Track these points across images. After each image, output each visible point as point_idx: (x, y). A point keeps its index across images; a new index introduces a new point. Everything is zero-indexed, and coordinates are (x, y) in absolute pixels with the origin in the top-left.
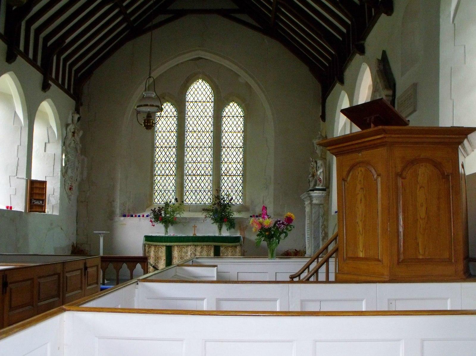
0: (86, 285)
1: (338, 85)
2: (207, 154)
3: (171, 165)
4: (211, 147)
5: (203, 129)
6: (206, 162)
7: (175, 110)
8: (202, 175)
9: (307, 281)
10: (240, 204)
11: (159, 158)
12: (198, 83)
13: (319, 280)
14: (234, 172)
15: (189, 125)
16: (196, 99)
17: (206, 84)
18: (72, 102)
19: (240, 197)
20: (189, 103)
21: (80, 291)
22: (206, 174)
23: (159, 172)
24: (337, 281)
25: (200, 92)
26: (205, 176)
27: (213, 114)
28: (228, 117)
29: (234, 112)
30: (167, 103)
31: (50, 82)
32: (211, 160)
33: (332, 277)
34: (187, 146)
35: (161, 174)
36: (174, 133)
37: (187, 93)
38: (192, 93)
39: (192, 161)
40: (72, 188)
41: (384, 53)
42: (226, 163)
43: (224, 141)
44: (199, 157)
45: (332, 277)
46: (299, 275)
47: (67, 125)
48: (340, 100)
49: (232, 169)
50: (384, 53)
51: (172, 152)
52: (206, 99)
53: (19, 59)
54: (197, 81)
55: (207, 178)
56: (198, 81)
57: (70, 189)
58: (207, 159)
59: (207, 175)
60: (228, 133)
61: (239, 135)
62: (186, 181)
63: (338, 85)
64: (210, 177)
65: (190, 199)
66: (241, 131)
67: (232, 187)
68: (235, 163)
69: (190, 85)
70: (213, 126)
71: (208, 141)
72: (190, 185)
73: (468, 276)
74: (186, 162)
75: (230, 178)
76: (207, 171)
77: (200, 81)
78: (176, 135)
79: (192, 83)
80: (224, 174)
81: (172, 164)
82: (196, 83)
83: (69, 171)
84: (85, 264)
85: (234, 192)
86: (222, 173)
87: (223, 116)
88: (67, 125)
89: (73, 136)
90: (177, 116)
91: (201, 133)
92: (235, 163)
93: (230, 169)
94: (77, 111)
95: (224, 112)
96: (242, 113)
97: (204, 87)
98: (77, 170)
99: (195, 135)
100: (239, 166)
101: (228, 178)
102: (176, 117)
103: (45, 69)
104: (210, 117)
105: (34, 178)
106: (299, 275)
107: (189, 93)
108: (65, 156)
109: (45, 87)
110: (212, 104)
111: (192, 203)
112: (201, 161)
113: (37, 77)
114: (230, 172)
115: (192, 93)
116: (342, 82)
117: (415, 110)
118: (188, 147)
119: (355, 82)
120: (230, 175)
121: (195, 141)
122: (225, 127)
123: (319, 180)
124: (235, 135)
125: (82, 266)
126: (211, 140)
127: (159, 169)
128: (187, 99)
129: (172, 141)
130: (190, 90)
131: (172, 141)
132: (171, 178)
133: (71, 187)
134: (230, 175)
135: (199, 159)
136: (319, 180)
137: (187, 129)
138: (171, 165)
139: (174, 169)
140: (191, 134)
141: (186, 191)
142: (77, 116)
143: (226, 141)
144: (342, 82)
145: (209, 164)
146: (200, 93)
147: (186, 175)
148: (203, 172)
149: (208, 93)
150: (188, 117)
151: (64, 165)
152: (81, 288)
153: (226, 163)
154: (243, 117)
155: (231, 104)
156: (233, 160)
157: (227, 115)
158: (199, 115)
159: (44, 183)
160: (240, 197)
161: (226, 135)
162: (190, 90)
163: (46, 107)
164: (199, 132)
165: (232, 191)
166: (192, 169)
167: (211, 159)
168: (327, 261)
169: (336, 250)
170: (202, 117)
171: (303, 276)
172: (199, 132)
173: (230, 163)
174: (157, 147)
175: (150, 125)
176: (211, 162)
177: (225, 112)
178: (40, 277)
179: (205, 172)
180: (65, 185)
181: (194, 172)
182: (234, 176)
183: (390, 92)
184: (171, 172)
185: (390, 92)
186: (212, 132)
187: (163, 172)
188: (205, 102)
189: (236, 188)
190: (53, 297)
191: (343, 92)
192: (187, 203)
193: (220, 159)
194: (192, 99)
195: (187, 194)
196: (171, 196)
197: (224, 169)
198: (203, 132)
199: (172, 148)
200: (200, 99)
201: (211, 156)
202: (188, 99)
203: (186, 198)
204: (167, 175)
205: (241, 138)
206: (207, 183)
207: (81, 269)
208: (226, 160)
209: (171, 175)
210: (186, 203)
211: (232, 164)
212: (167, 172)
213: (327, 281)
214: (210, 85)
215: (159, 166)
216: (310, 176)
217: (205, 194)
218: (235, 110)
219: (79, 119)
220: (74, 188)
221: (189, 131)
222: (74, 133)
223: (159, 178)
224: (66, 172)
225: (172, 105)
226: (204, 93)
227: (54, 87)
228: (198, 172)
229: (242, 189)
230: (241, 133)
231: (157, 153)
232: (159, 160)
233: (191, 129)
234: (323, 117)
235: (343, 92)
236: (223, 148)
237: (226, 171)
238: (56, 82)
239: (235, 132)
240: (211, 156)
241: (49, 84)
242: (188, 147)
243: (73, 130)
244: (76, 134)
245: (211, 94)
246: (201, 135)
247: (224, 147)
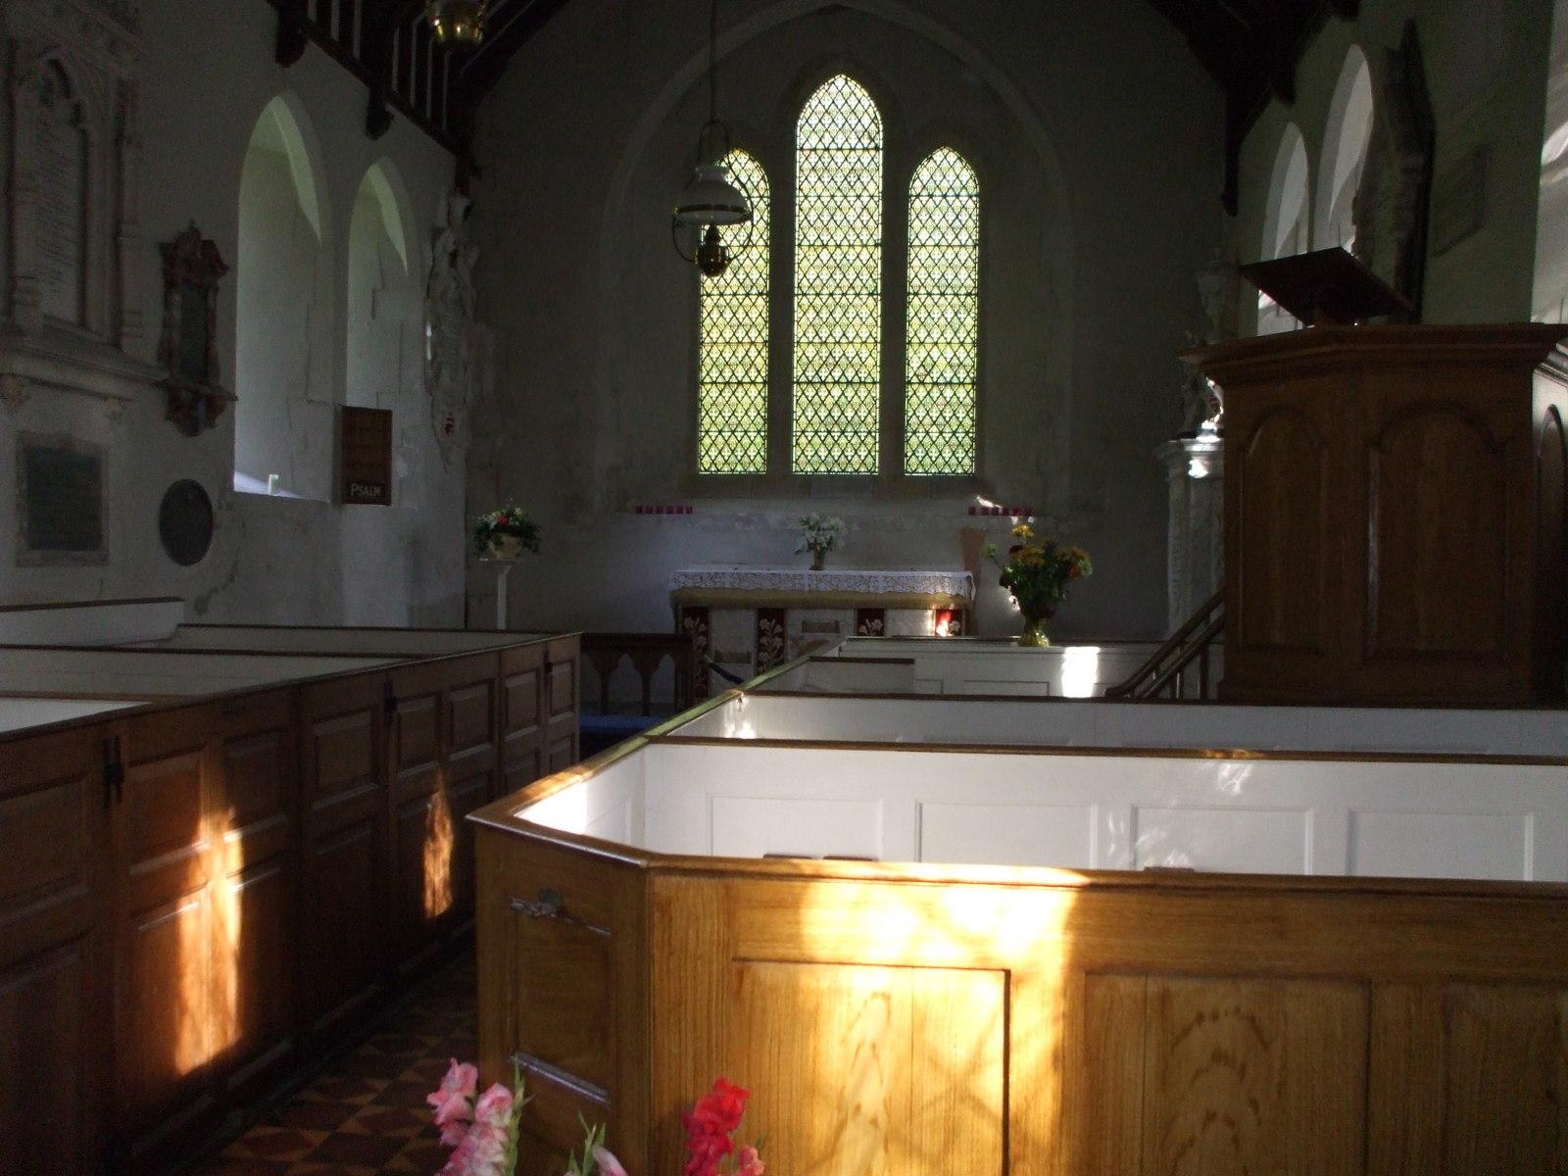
0: (1029, 649)
1: (1275, 107)
2: (864, 316)
3: (753, 353)
4: (877, 294)
5: (852, 237)
6: (807, 243)
7: (763, 178)
8: (849, 383)
9: (1154, 698)
10: (966, 472)
11: (715, 328)
12: (833, 89)
13: (1185, 697)
14: (949, 375)
15: (805, 223)
16: (827, 140)
17: (857, 91)
18: (443, 161)
19: (967, 452)
20: (807, 153)
21: (534, 728)
22: (860, 378)
23: (714, 374)
24: (1225, 699)
25: (840, 119)
26: (856, 387)
27: (881, 189)
28: (927, 198)
29: (946, 182)
30: (737, 152)
31: (390, 108)
32: (875, 335)
33: (1213, 694)
34: (800, 292)
35: (720, 380)
36: (761, 249)
37: (800, 122)
38: (814, 121)
39: (817, 340)
40: (647, 507)
41: (1411, 29)
42: (921, 343)
43: (916, 276)
44: (838, 328)
45: (1213, 694)
46: (1131, 689)
47: (435, 234)
48: (1281, 151)
49: (942, 363)
50: (1411, 29)
51: (754, 310)
52: (857, 140)
53: (313, 50)
54: (830, 82)
55: (863, 392)
56: (833, 82)
57: (448, 428)
58: (864, 334)
59: (865, 383)
60: (930, 249)
61: (963, 254)
62: (797, 401)
63: (1275, 107)
64: (873, 389)
65: (809, 455)
66: (970, 242)
67: (941, 420)
68: (949, 343)
69: (807, 97)
70: (880, 226)
71: (865, 276)
72: (810, 413)
73: (1547, 694)
74: (798, 342)
75: (935, 393)
76: (863, 370)
77: (840, 80)
78: (764, 256)
79: (814, 88)
80: (915, 380)
81: (753, 347)
82: (826, 88)
83: (445, 373)
84: (546, 655)
85: (947, 436)
86: (911, 375)
87: (914, 193)
88: (435, 234)
89: (453, 262)
90: (767, 197)
91: (845, 249)
92: (949, 343)
93: (935, 363)
94: (461, 186)
95: (914, 180)
96: (971, 184)
97: (853, 102)
98: (466, 369)
99: (825, 255)
100: (962, 354)
101: (928, 393)
102: (765, 199)
103: (370, 68)
104: (872, 197)
105: (354, 400)
106: (1131, 689)
107: (804, 120)
108: (433, 328)
109: (376, 123)
110: (879, 157)
111: (816, 471)
112: (844, 340)
113: (353, 92)
114: (935, 374)
115: (814, 121)
116: (1288, 96)
117: (1476, 227)
118: (804, 295)
119: (1327, 107)
120: (935, 384)
121: (825, 276)
122: (919, 230)
123: (1213, 402)
124: (950, 254)
125: (539, 662)
126: (875, 273)
127: (711, 358)
128: (800, 141)
129: (755, 275)
130: (809, 110)
131: (755, 275)
132: (753, 391)
133: (450, 422)
134: (935, 384)
135: (838, 333)
136: (1213, 402)
137: (801, 238)
138: (753, 353)
139: (760, 362)
140: (812, 255)
141: (799, 434)
142: (460, 205)
143: (923, 275)
144: (1288, 96)
145: (871, 347)
146: (840, 121)
147: (798, 383)
148: (850, 374)
149: (866, 121)
150: (802, 199)
151: (429, 357)
152: (537, 721)
153: (921, 343)
154: (974, 198)
155: (938, 156)
156: (945, 337)
157: (925, 193)
158: (839, 194)
159: (386, 415)
160: (967, 452)
161: (923, 254)
162: (809, 110)
163: (378, 182)
164: (838, 246)
165: (941, 433)
166: (817, 362)
167: (878, 333)
168: (1203, 649)
169: (1221, 625)
170: (846, 197)
171: (1139, 690)
172: (838, 246)
173: (936, 344)
174: (709, 295)
175: (716, 263)
176: (876, 342)
177: (918, 180)
178: (453, 688)
179: (857, 374)
180: (433, 417)
181: (823, 374)
182: (946, 384)
183: (1417, 161)
184: (753, 374)
185: (1417, 161)
186: (876, 245)
187: (727, 374)
188: (854, 149)
189: (954, 423)
190: (478, 742)
191: (1292, 129)
192: (802, 471)
193: (903, 331)
194: (814, 141)
195: (803, 440)
196: (753, 447)
197: (915, 363)
198: (850, 246)
199: (753, 298)
200: (840, 140)
201: (876, 322)
202: (802, 142)
203: (799, 453)
204: (740, 383)
205: (970, 263)
206: (865, 404)
207: (537, 670)
208: (922, 334)
209: (753, 383)
210: (798, 469)
211: (942, 347)
212: (740, 373)
213: (1204, 700)
214: (873, 95)
215: (715, 354)
216: (1184, 387)
217: (855, 440)
218: (951, 177)
219: (468, 211)
220: (457, 425)
221: (805, 242)
222: (454, 255)
223: (714, 392)
224: (437, 377)
225: (753, 161)
226: (853, 121)
227: (400, 122)
228: (837, 374)
229: (973, 425)
230: (970, 249)
231: (709, 314)
232: (715, 334)
233: (812, 236)
234: (1231, 199)
235: (1292, 129)
236: (912, 297)
237: (922, 370)
238: (402, 107)
239: (949, 245)
240: (876, 322)
241: (388, 113)
242: (804, 295)
243: (451, 248)
244: (460, 261)
245: (873, 125)
246: (858, 276)
247: (916, 294)
